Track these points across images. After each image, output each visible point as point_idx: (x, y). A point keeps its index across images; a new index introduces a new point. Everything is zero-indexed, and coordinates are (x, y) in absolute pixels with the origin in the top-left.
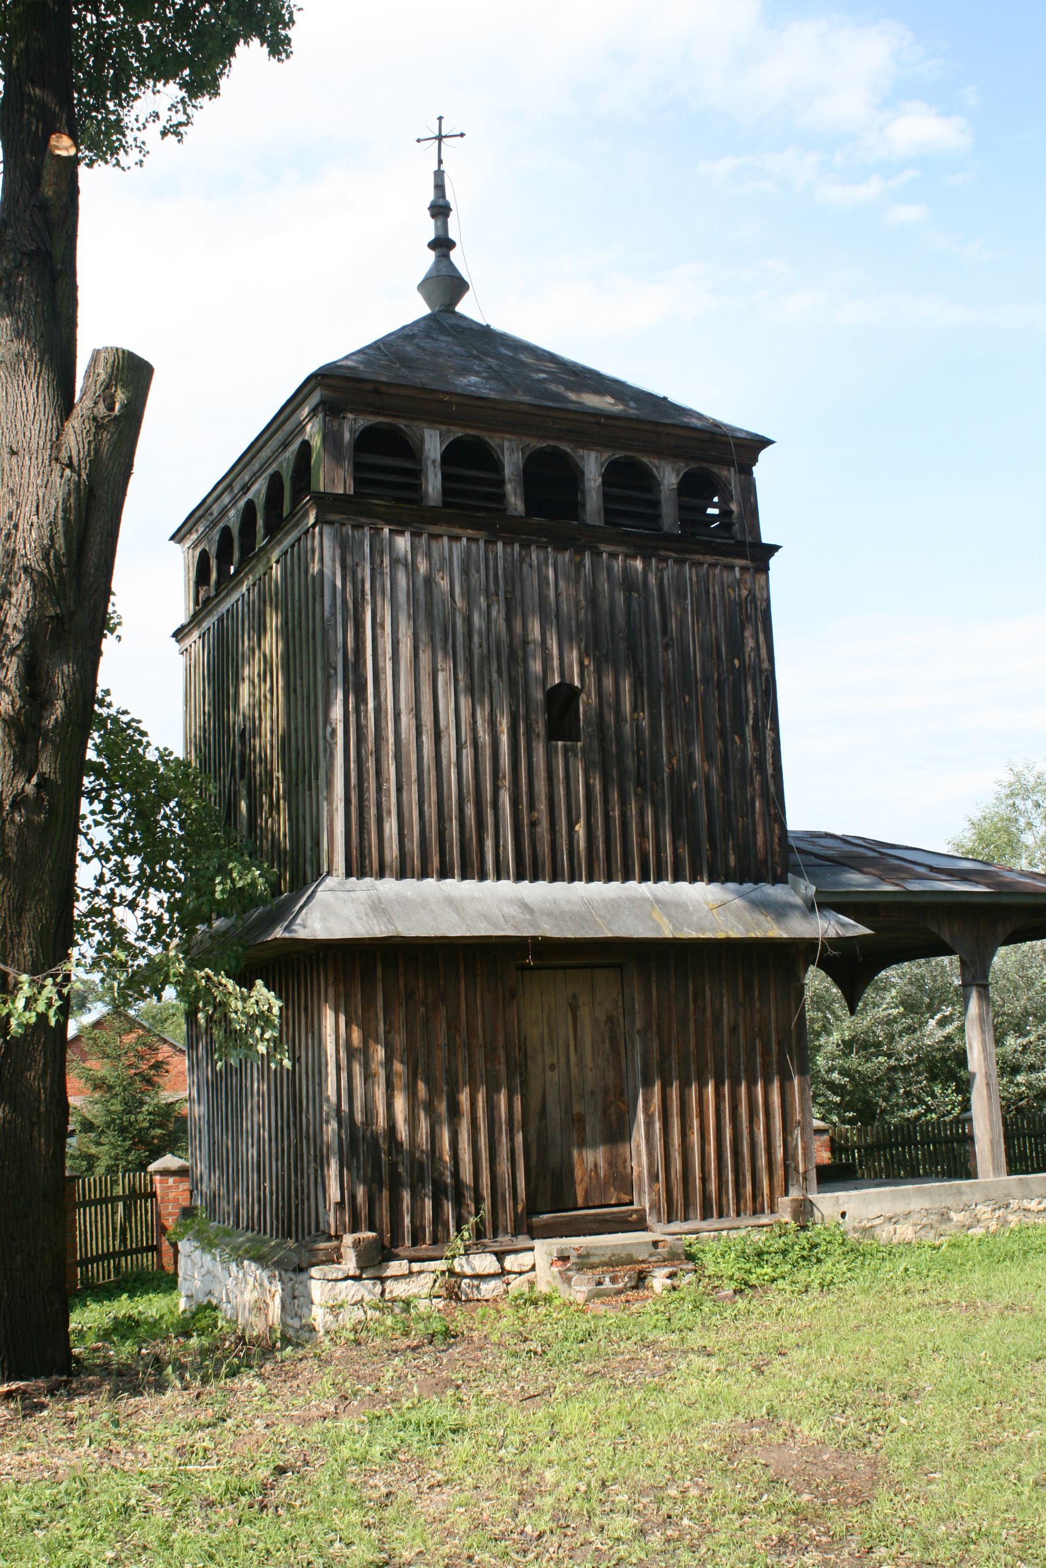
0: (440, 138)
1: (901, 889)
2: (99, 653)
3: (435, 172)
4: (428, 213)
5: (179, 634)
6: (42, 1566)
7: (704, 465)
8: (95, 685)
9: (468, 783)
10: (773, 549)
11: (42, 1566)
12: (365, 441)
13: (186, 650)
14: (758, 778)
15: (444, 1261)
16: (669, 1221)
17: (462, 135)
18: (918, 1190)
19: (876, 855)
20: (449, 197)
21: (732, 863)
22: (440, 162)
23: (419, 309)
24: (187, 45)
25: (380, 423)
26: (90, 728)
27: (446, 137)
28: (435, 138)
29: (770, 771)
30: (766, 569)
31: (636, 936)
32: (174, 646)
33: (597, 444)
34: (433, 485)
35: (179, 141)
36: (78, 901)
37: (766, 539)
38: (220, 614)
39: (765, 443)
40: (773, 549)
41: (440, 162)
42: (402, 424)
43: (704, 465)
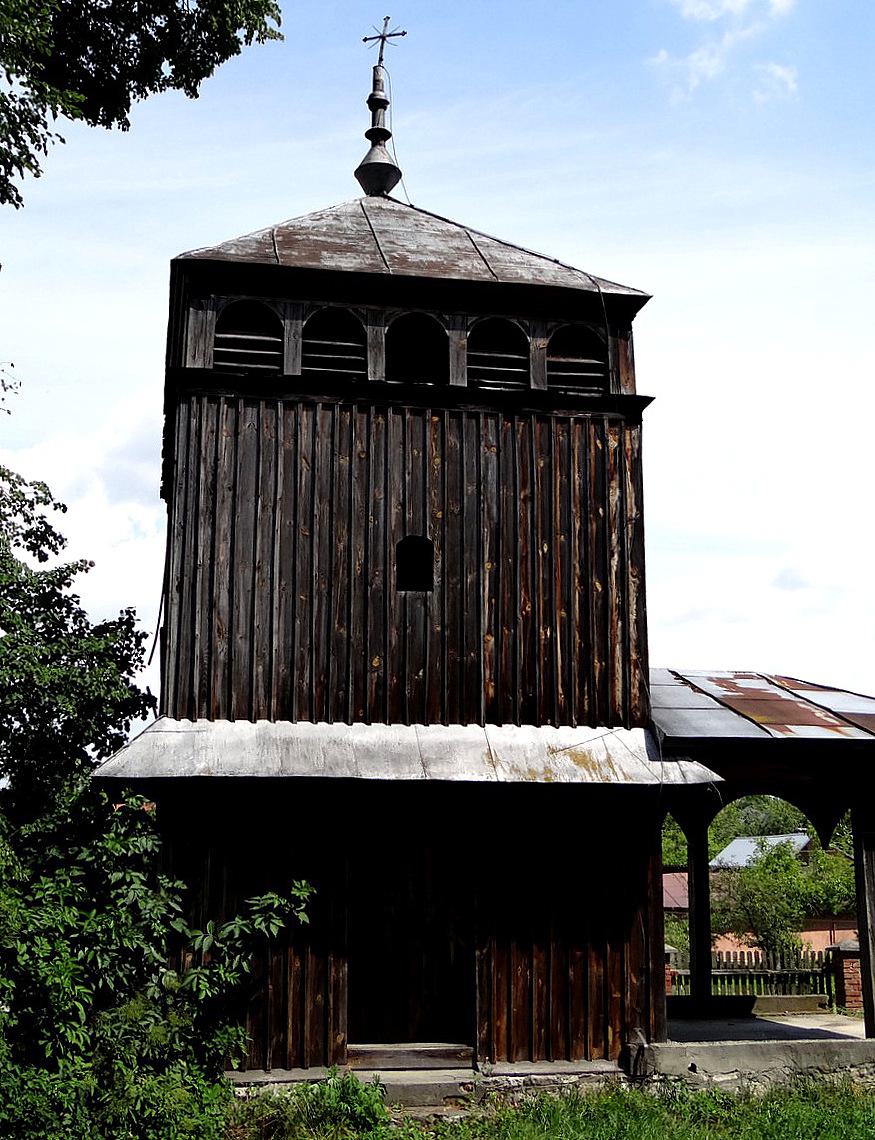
0: (383, 38)
1: (770, 736)
6: (4, 145)
9: (592, 533)
10: (648, 400)
11: (4, 145)
14: (620, 624)
17: (404, 33)
18: (713, 1050)
19: (793, 698)
21: (586, 708)
22: (381, 59)
26: (229, 33)
27: (390, 35)
28: (380, 37)
29: (633, 617)
30: (639, 421)
31: (175, 775)
37: (641, 391)
41: (381, 59)
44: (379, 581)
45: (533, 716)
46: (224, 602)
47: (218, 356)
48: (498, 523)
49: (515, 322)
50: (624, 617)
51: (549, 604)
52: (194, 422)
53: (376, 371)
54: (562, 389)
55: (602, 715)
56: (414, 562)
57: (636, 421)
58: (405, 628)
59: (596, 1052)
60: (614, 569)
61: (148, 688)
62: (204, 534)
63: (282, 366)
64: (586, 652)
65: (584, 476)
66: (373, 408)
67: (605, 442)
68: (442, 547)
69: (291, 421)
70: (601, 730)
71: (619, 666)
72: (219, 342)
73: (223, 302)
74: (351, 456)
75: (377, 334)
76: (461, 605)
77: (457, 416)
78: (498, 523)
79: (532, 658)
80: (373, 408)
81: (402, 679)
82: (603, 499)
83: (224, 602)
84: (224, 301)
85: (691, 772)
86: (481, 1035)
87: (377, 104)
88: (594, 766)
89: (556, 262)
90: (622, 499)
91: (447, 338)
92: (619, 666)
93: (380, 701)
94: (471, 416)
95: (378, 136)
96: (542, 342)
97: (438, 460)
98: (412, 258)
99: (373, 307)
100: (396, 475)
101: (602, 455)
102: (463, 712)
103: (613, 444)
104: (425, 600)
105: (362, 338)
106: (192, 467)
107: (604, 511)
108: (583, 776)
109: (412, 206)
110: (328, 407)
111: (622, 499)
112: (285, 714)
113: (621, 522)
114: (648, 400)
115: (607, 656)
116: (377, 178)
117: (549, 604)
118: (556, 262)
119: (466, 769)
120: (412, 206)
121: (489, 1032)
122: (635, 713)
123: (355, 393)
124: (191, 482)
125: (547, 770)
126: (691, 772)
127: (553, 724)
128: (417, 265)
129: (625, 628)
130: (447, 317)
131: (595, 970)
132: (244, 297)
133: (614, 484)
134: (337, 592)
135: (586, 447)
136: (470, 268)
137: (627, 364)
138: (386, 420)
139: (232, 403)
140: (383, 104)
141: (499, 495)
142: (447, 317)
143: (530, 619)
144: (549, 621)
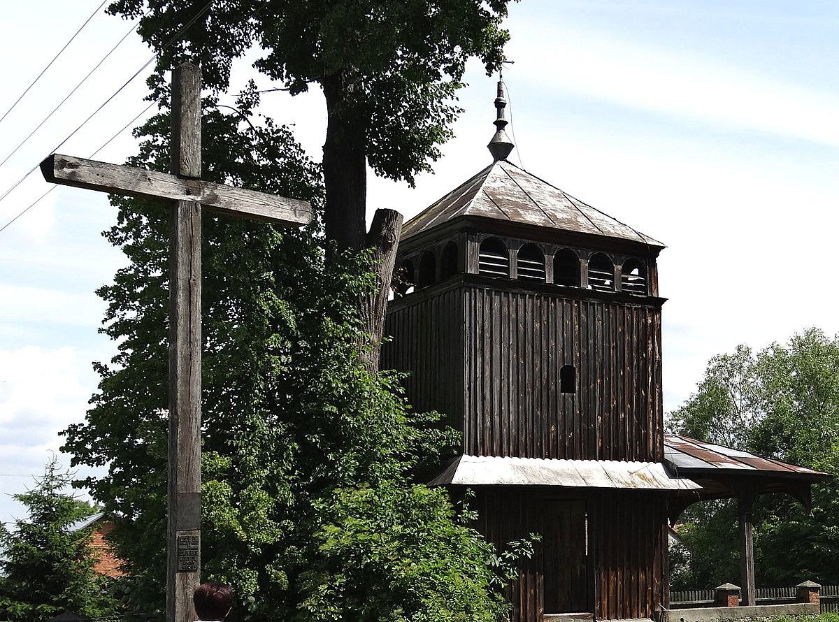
10: (665, 300)
17: (513, 63)
37: (661, 295)
44: (553, 387)
45: (618, 456)
46: (488, 396)
47: (482, 266)
48: (603, 360)
49: (608, 255)
50: (654, 409)
51: (623, 400)
52: (473, 301)
53: (549, 279)
54: (631, 292)
55: (644, 457)
56: (568, 376)
57: (659, 311)
58: (565, 412)
59: (642, 615)
60: (650, 381)
61: (60, 434)
62: (479, 360)
63: (508, 273)
64: (638, 425)
65: (638, 338)
66: (550, 298)
67: (646, 320)
68: (579, 371)
69: (514, 303)
70: (645, 464)
71: (651, 433)
72: (482, 259)
73: (482, 237)
74: (541, 323)
75: (549, 259)
76: (588, 399)
77: (585, 304)
78: (603, 360)
79: (617, 427)
80: (550, 298)
81: (564, 437)
82: (646, 350)
83: (488, 396)
84: (482, 238)
85: (688, 484)
86: (597, 608)
87: (500, 105)
88: (649, 481)
89: (615, 219)
90: (653, 349)
91: (580, 262)
92: (651, 433)
93: (616, 450)
94: (591, 304)
95: (500, 125)
96: (620, 267)
97: (577, 326)
98: (560, 216)
99: (548, 244)
100: (560, 334)
101: (646, 324)
102: (589, 453)
103: (650, 321)
104: (573, 397)
105: (543, 260)
106: (473, 326)
107: (646, 355)
108: (646, 486)
109: (524, 170)
110: (531, 297)
111: (653, 349)
112: (517, 455)
113: (653, 361)
114: (665, 300)
115: (647, 428)
116: (500, 150)
117: (623, 400)
118: (615, 219)
119: (600, 481)
120: (524, 170)
121: (600, 605)
122: (656, 456)
123: (536, 287)
124: (473, 334)
125: (633, 483)
126: (688, 484)
127: (625, 460)
128: (562, 221)
129: (654, 414)
130: (580, 251)
131: (642, 577)
132: (492, 235)
133: (650, 342)
134: (536, 392)
135: (638, 322)
136: (585, 227)
137: (654, 279)
138: (555, 305)
139: (489, 293)
140: (503, 105)
141: (603, 345)
142: (580, 251)
143: (616, 408)
144: (624, 410)
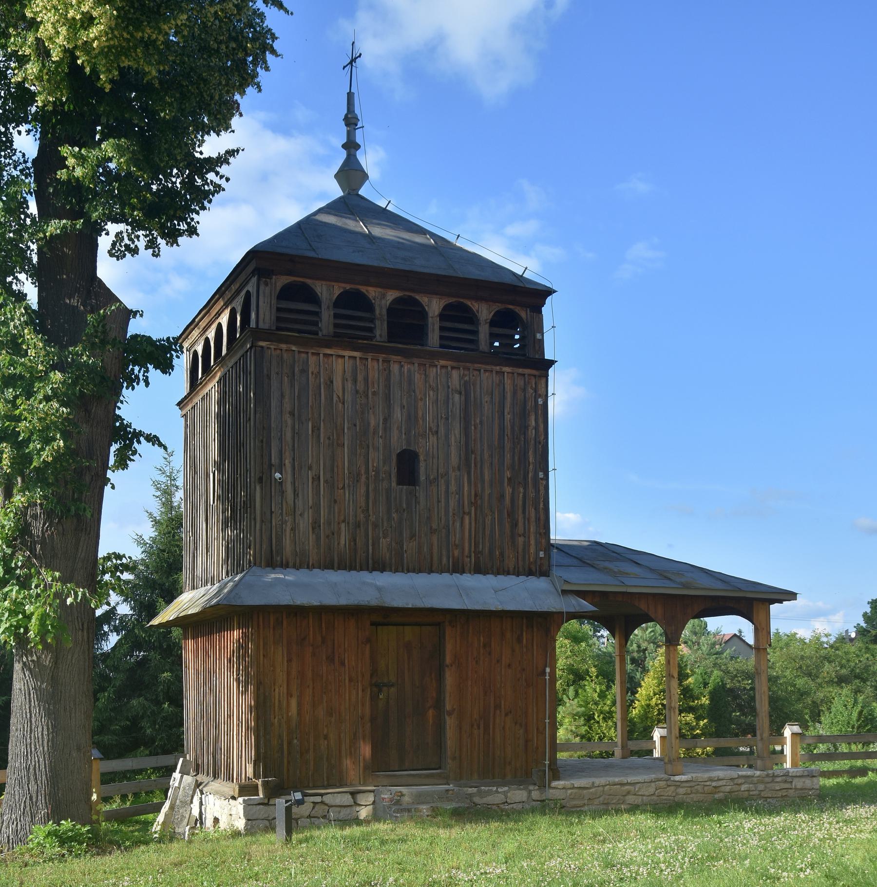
2: (97, 245)
3: (348, 93)
4: (343, 123)
5: (181, 404)
7: (511, 307)
8: (97, 556)
10: (552, 363)
12: (286, 293)
13: (185, 415)
15: (352, 801)
16: (493, 778)
20: (357, 111)
23: (336, 191)
24: (165, 116)
25: (295, 281)
32: (178, 412)
33: (436, 294)
34: (327, 321)
35: (141, 316)
36: (130, 385)
37: (548, 356)
38: (203, 395)
39: (549, 292)
40: (552, 363)
42: (309, 282)
43: (511, 307)
